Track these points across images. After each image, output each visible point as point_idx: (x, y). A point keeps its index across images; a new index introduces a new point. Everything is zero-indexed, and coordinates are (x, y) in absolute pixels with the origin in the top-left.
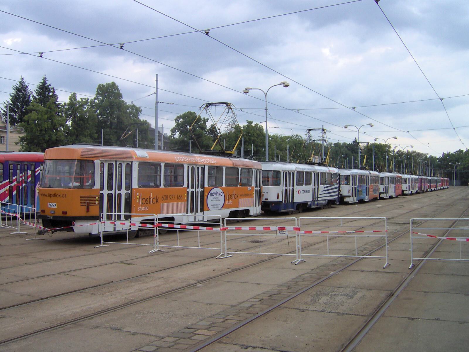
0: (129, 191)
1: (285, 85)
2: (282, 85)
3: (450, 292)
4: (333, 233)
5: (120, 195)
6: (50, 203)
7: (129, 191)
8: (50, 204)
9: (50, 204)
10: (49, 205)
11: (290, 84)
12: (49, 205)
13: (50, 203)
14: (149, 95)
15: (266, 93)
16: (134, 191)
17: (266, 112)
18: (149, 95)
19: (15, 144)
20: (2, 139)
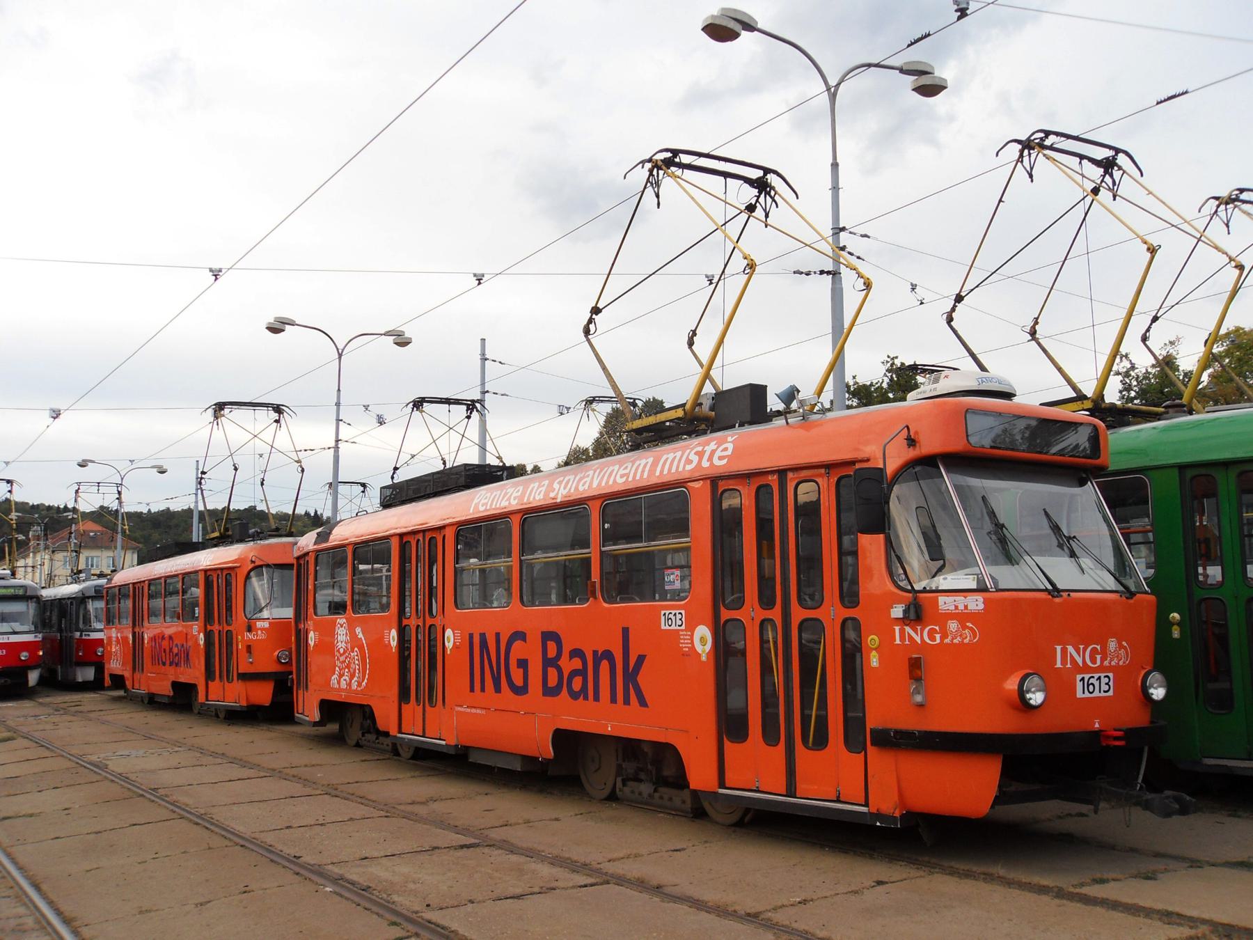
0: (726, 614)
1: (925, 80)
2: (910, 80)
3: (92, 836)
4: (409, 649)
5: (766, 601)
6: (1087, 677)
7: (726, 614)
8: (1083, 679)
9: (1083, 679)
10: (1079, 685)
11: (949, 84)
12: (1079, 685)
13: (1087, 677)
14: (862, 236)
15: (341, 347)
16: (708, 611)
17: (1039, 344)
18: (862, 236)
19: (475, 415)
20: (228, 624)
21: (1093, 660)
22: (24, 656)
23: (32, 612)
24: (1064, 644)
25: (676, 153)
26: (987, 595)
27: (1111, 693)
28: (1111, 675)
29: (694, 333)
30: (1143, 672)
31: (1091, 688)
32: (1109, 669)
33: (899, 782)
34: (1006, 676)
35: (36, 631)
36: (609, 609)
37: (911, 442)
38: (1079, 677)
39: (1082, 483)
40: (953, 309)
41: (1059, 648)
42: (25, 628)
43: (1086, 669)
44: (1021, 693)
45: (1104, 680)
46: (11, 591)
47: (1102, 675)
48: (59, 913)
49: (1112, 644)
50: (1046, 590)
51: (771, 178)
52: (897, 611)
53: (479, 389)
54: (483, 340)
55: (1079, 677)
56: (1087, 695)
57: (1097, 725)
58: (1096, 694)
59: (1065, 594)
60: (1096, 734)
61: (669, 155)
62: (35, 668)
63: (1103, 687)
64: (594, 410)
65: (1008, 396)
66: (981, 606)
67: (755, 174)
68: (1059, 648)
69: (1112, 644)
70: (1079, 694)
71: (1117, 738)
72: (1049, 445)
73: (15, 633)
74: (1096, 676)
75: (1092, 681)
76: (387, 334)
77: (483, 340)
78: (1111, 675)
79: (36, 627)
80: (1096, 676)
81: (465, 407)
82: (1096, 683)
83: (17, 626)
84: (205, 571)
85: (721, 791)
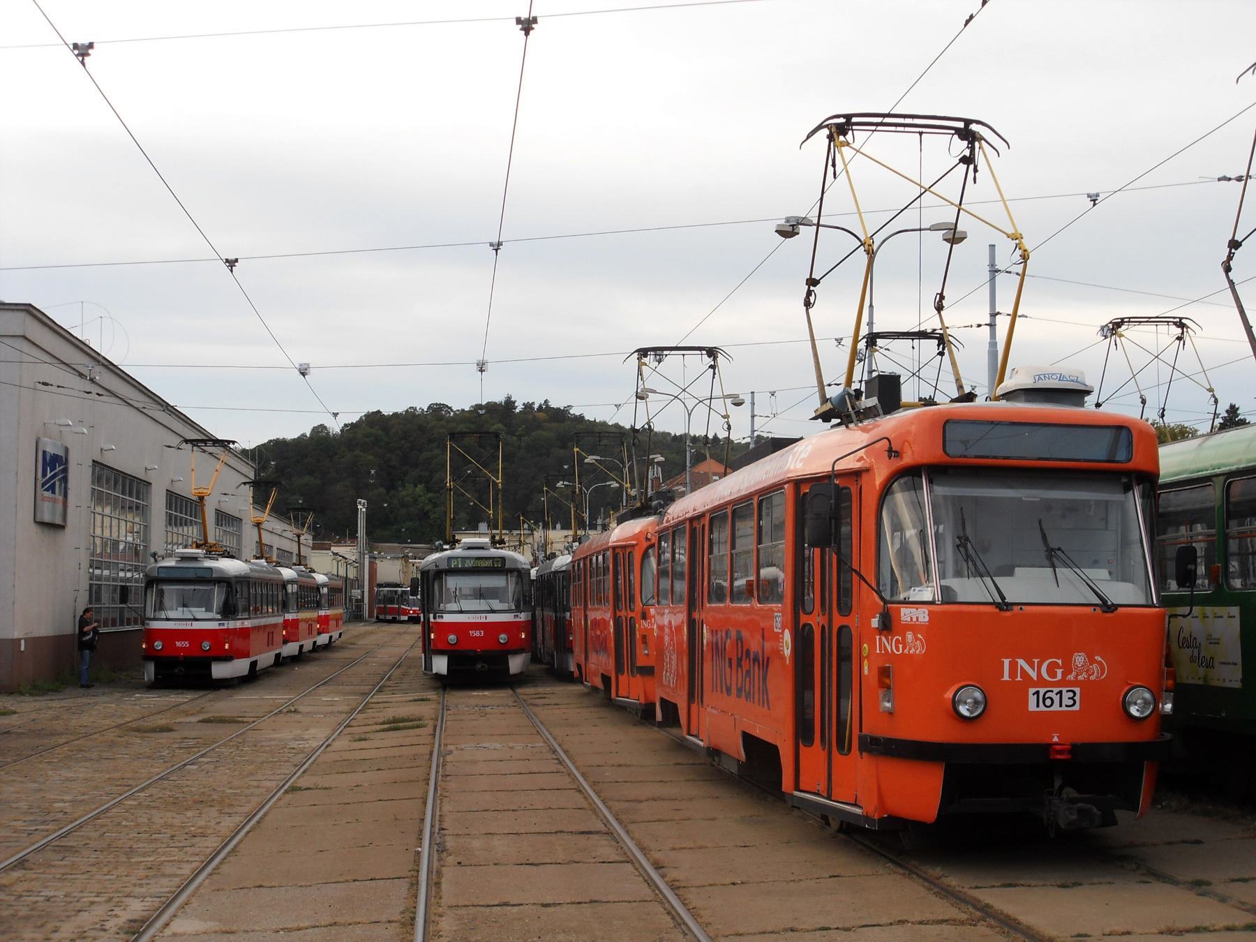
6: (1042, 690)
8: (1037, 693)
10: (1032, 700)
12: (1032, 700)
13: (1042, 690)
21: (1051, 672)
22: (503, 638)
23: (511, 588)
24: (1014, 656)
25: (848, 117)
26: (932, 608)
27: (1077, 707)
28: (1077, 690)
29: (942, 297)
30: (1126, 688)
31: (1048, 702)
32: (1075, 683)
33: (879, 788)
34: (946, 689)
35: (518, 609)
36: (762, 609)
37: (892, 453)
38: (1032, 690)
39: (1127, 488)
40: (1230, 257)
41: (1006, 662)
42: (505, 606)
43: (1041, 682)
44: (955, 704)
45: (1066, 695)
46: (488, 564)
47: (1064, 690)
48: (239, 843)
49: (1079, 659)
50: (994, 603)
51: (974, 127)
52: (875, 623)
53: (987, 311)
54: (992, 247)
55: (1032, 690)
56: (1042, 708)
57: (1056, 739)
58: (1056, 707)
59: (1016, 608)
60: (1048, 747)
61: (842, 120)
62: (516, 652)
63: (1065, 702)
64: (1121, 336)
65: (1076, 395)
66: (927, 619)
67: (961, 125)
68: (1006, 662)
69: (1079, 659)
70: (1032, 706)
71: (1060, 752)
72: (670, 498)
73: (493, 611)
74: (1056, 690)
75: (1048, 695)
76: (934, 228)
77: (992, 247)
78: (1077, 690)
79: (517, 606)
80: (1056, 690)
81: (936, 342)
82: (1053, 699)
83: (496, 604)
84: (614, 548)
85: (796, 793)
